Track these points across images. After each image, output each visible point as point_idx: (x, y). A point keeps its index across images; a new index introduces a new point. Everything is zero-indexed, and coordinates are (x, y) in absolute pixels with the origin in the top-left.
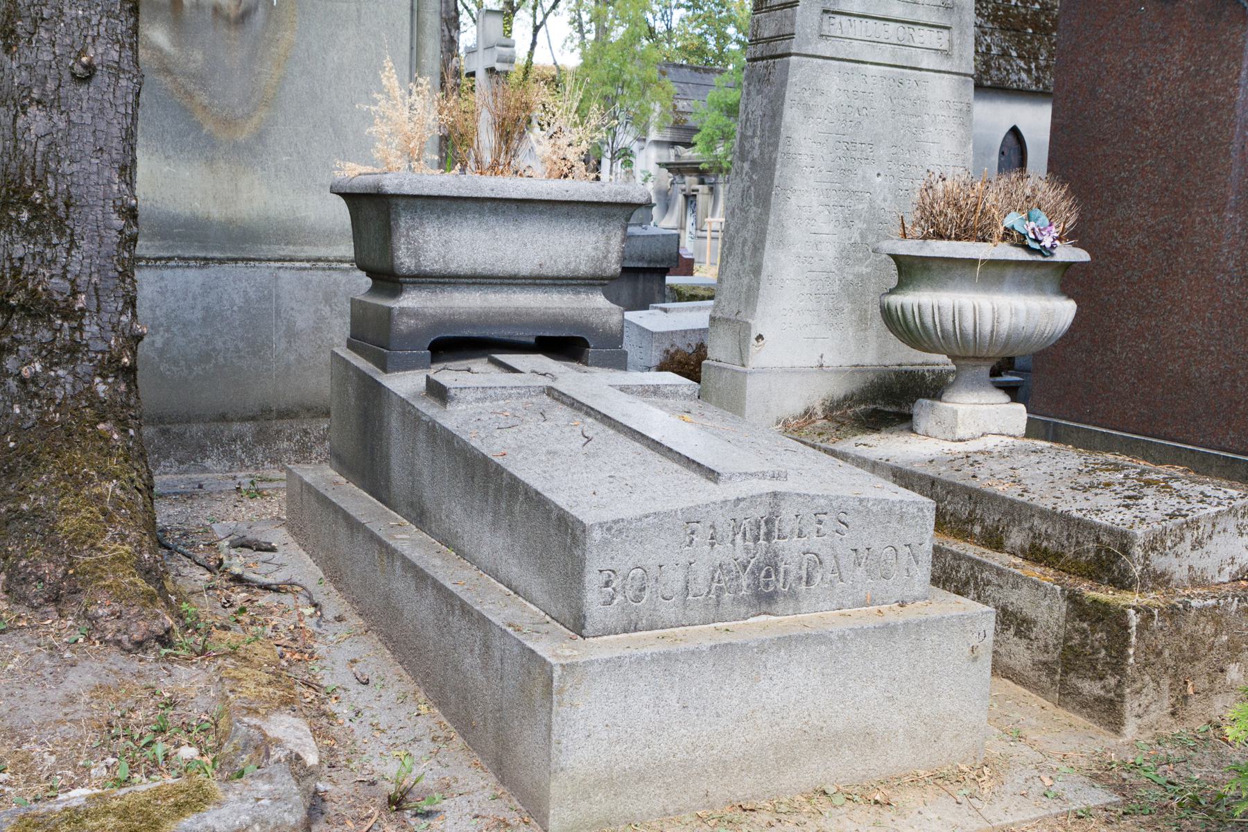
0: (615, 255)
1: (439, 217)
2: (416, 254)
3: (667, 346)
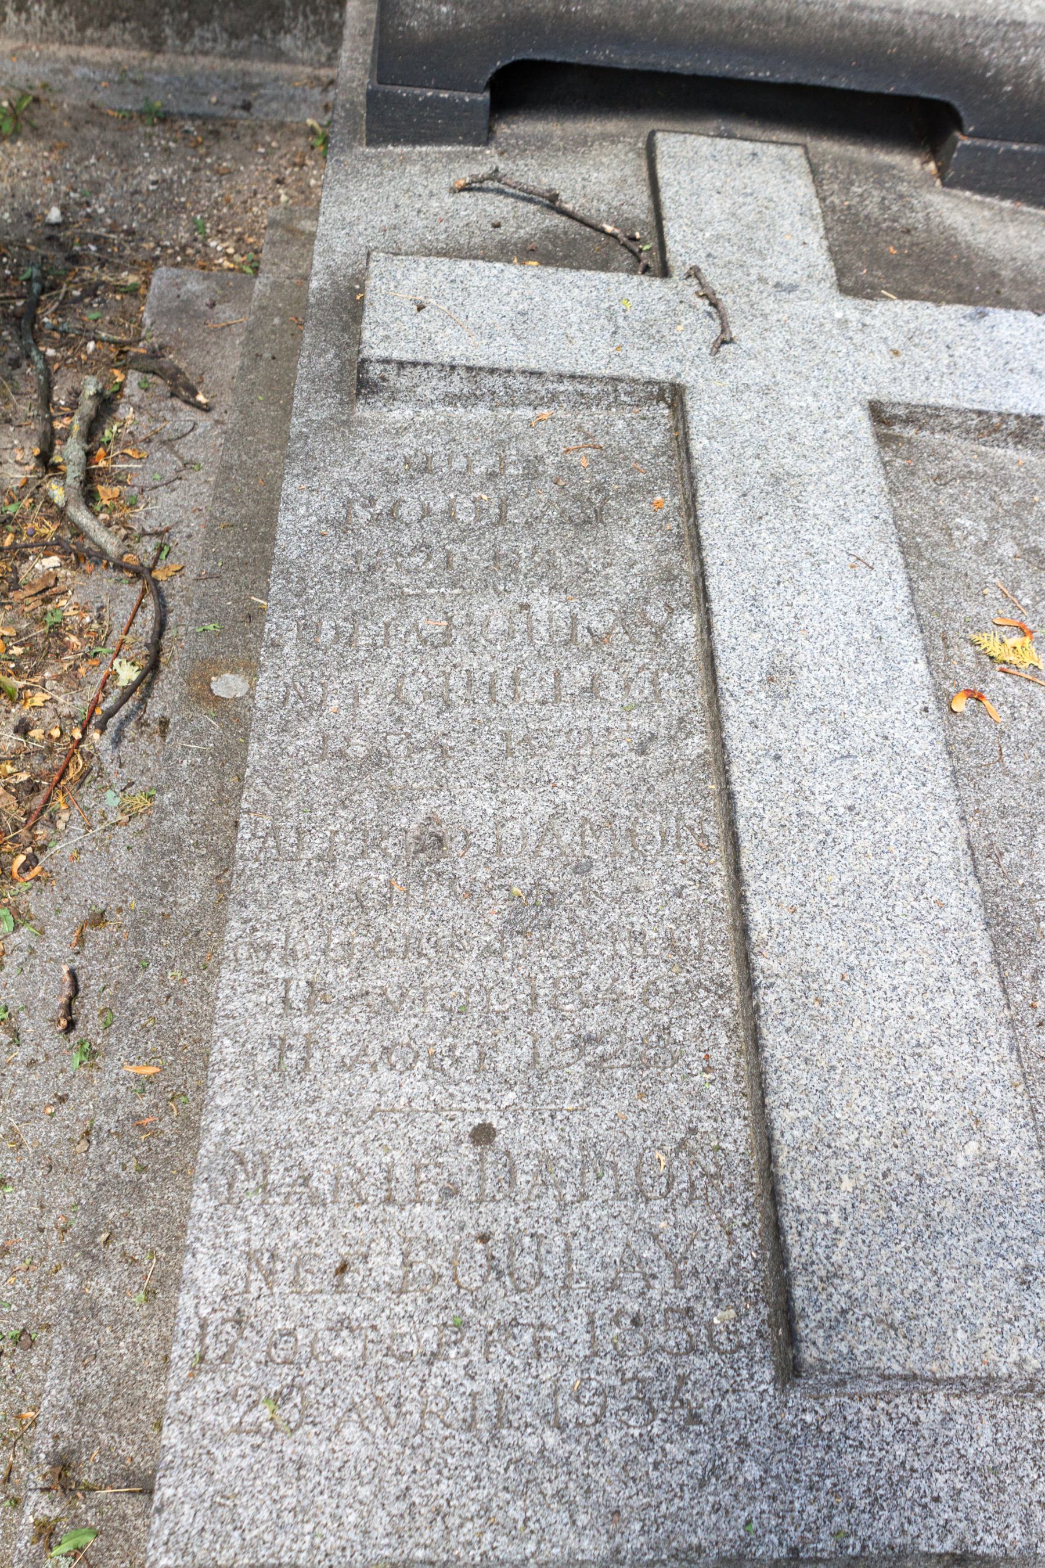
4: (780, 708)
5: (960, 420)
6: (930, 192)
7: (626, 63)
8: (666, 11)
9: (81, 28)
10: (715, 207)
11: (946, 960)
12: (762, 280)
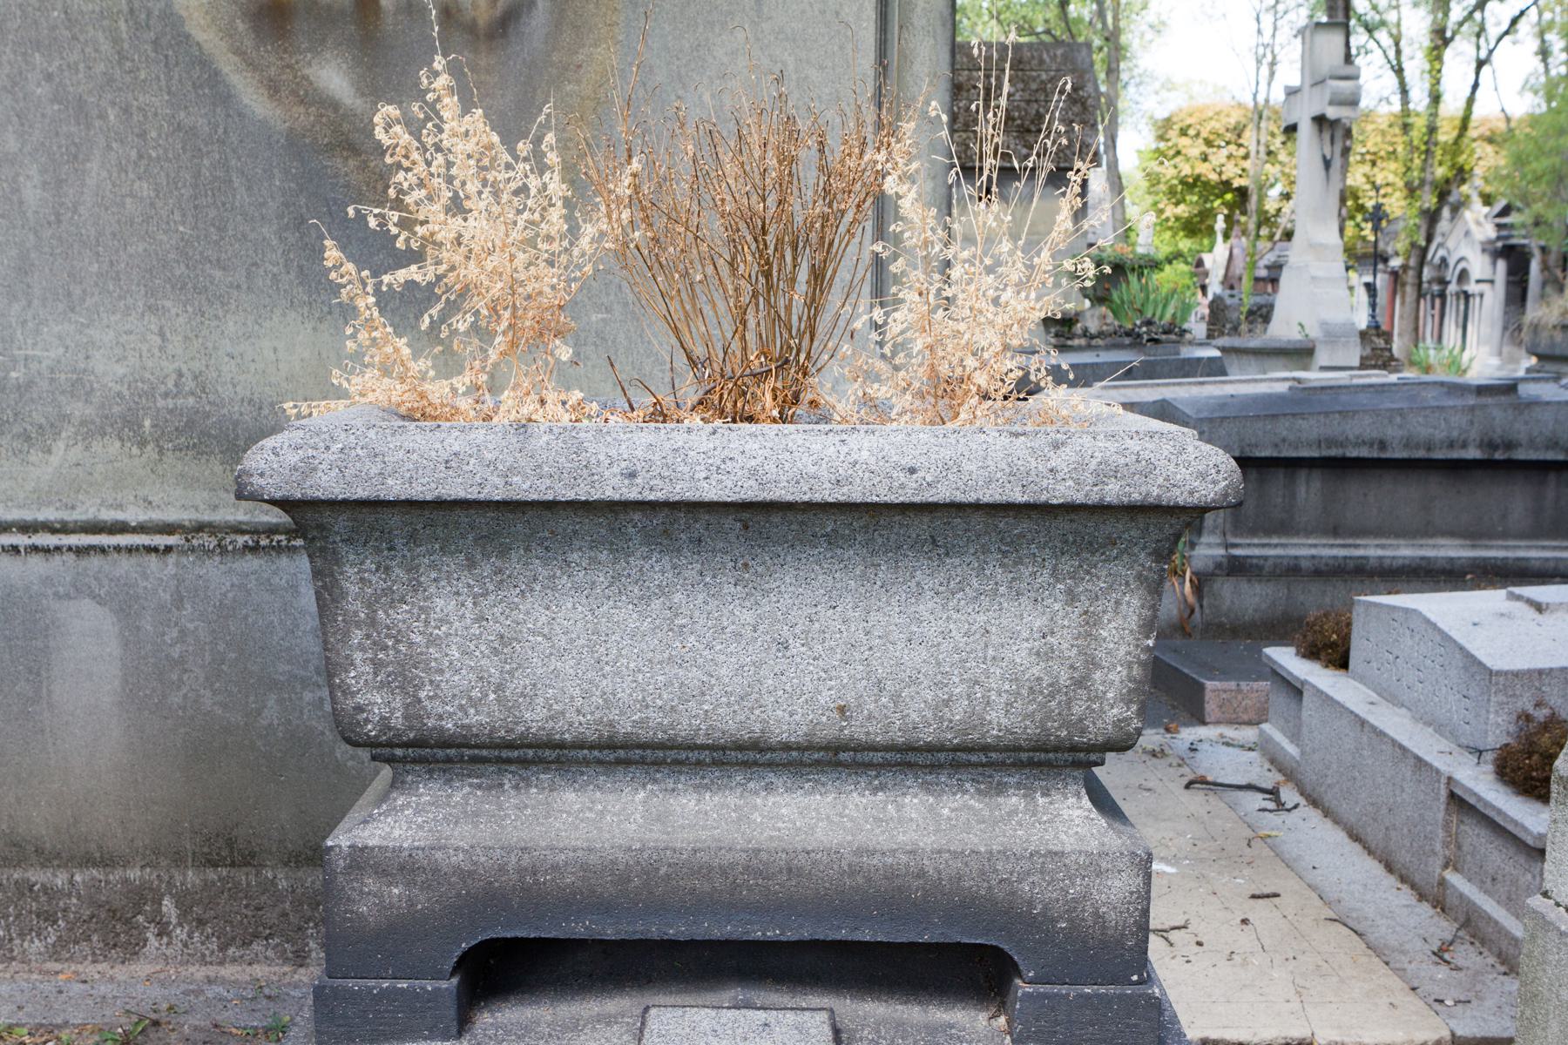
0: (1118, 675)
1: (472, 564)
2: (402, 678)
3: (1526, 703)
7: (610, 933)
8: (647, 873)
9: (223, 948)
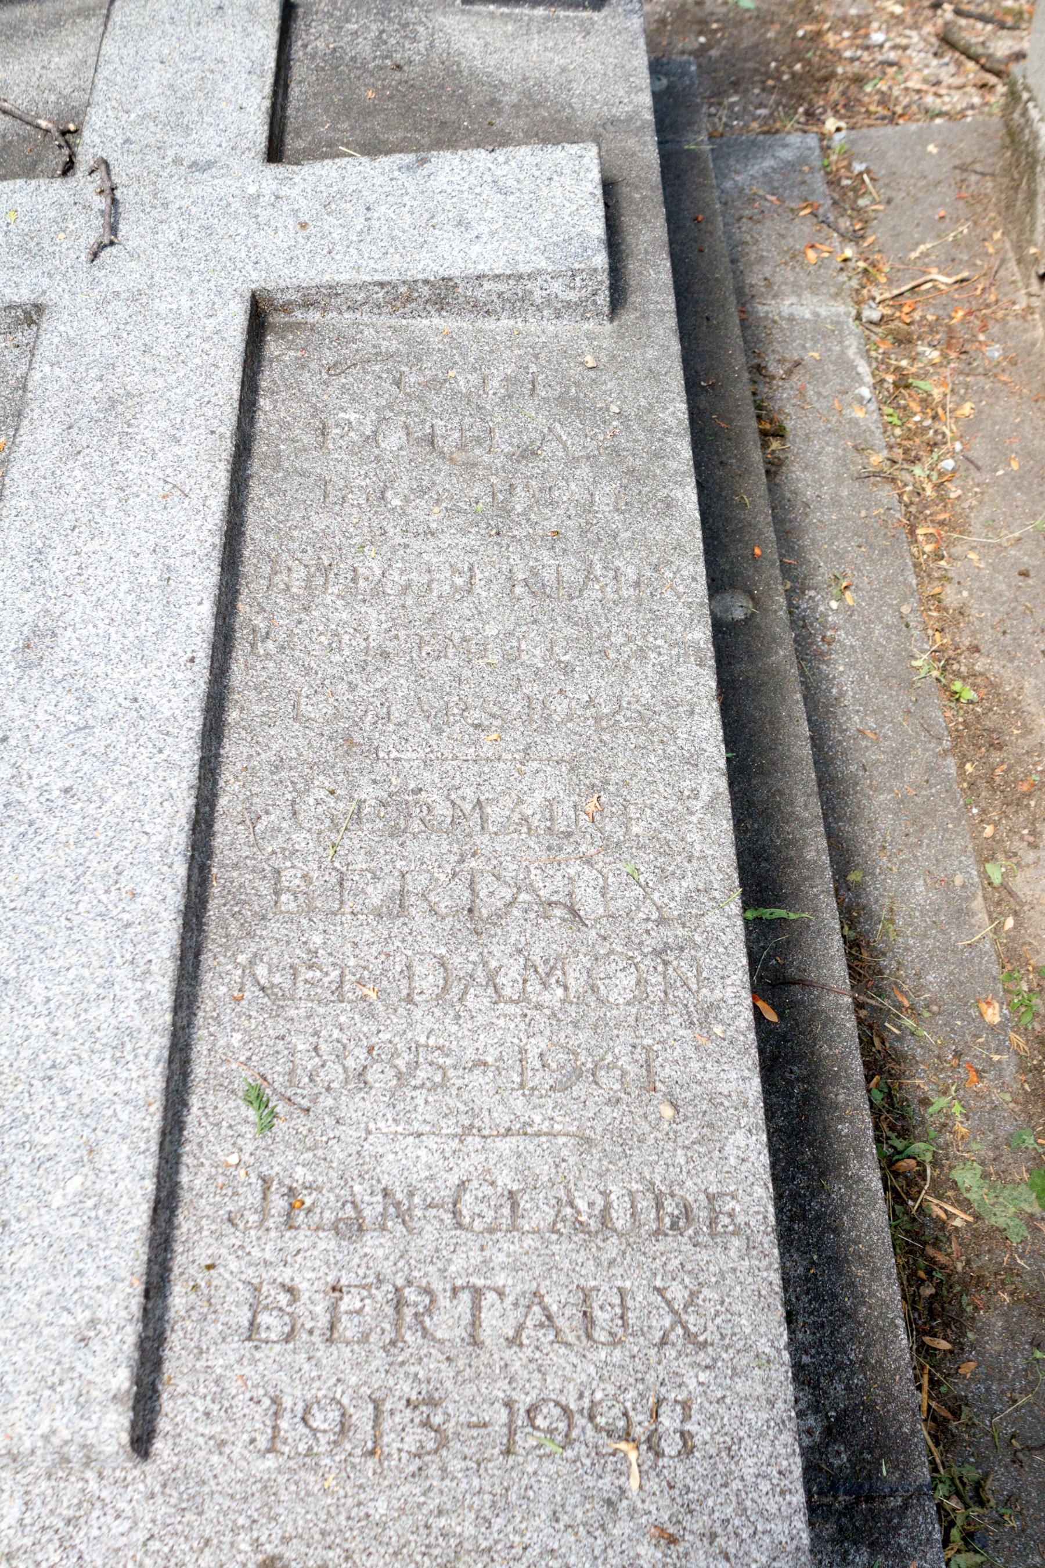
4: (26, 678)
5: (363, 295)
6: (444, 14)
10: (154, 79)
11: (119, 961)
12: (177, 161)
